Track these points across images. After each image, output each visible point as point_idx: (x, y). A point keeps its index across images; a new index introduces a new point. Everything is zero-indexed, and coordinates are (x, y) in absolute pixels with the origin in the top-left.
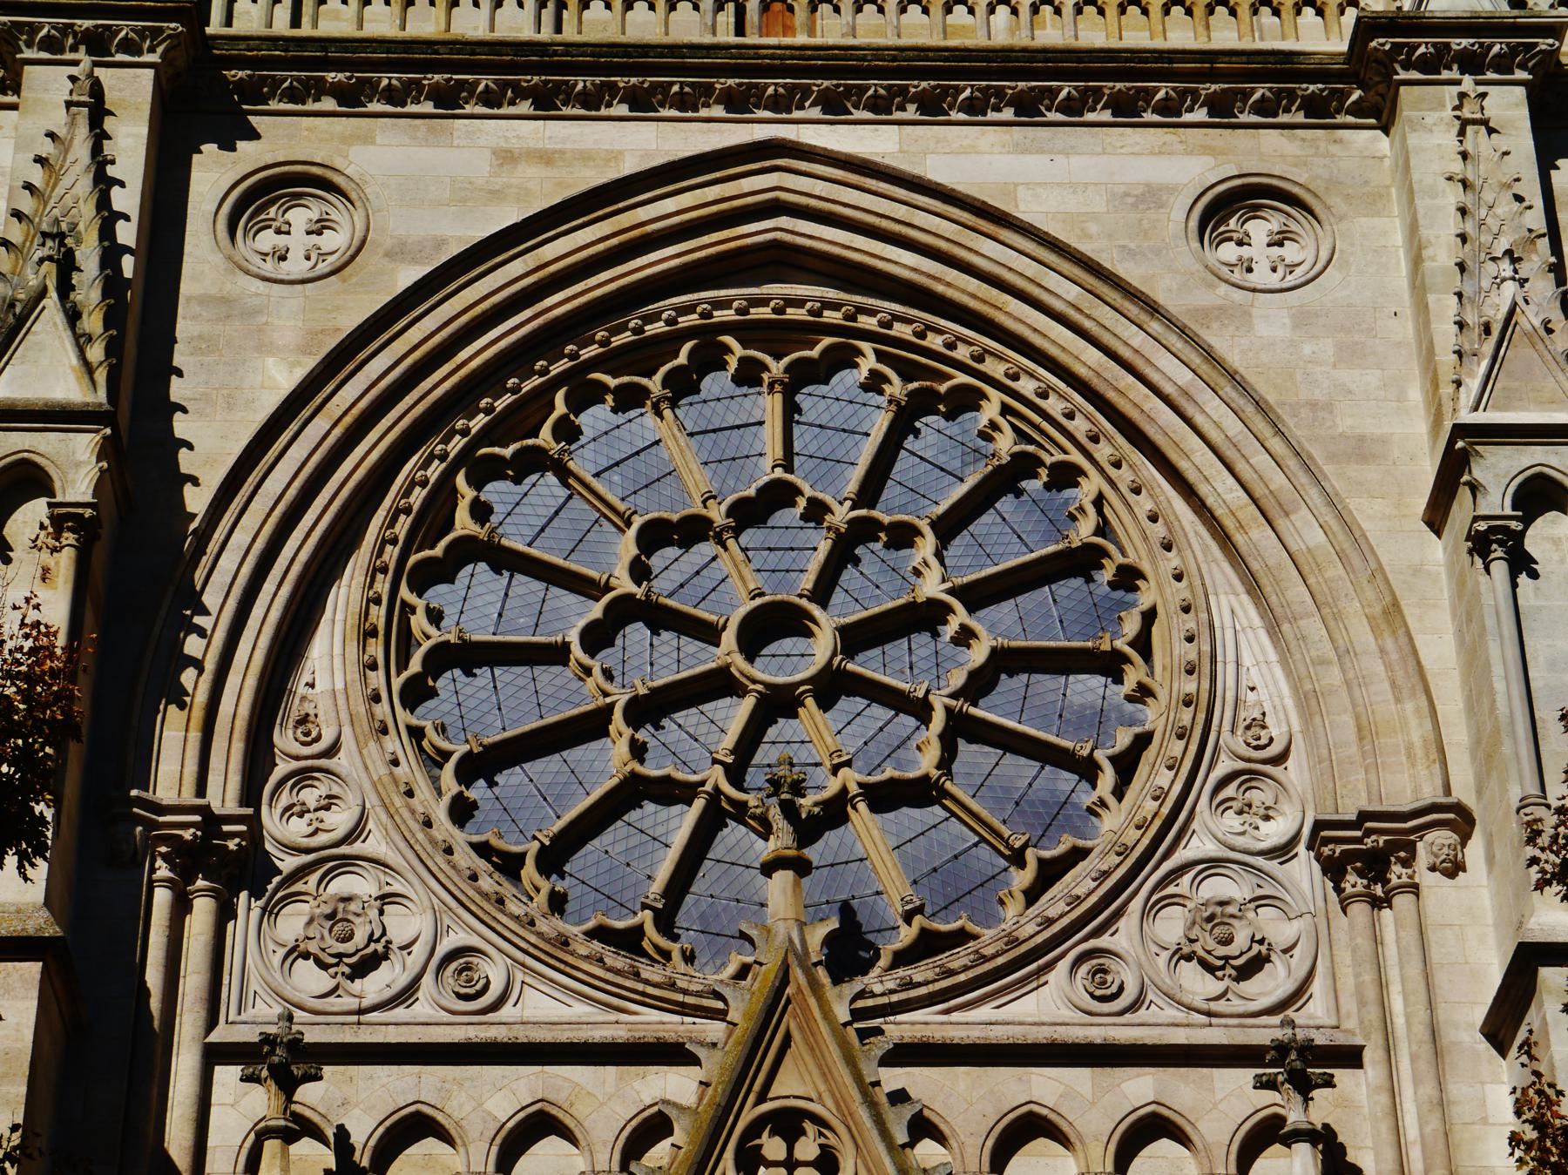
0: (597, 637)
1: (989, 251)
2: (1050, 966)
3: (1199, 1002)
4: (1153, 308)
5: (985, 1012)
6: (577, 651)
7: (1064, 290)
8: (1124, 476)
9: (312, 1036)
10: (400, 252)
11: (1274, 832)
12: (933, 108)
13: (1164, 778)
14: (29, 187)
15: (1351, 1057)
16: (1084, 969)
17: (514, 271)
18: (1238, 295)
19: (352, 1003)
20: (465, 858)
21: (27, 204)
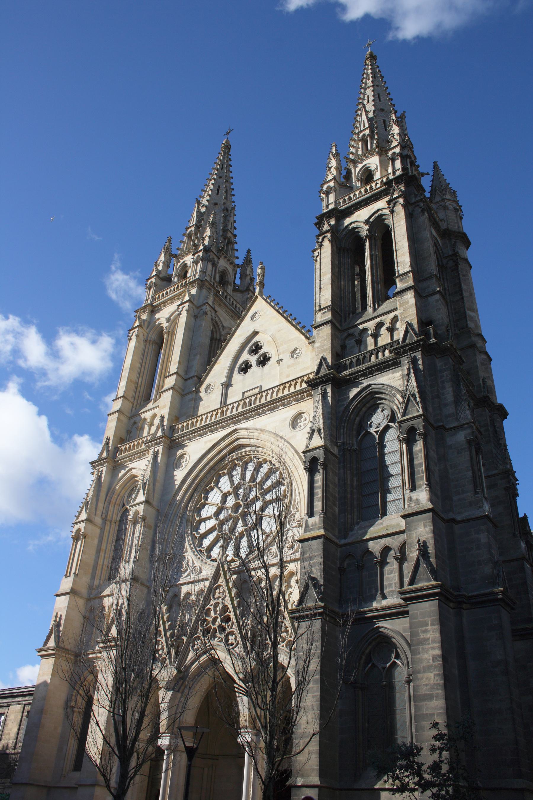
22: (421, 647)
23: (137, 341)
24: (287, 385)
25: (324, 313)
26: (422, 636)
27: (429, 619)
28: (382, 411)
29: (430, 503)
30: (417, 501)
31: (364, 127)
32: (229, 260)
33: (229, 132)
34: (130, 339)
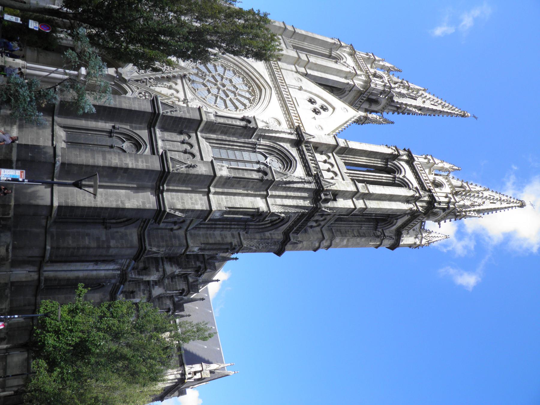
5: (188, 91)
22: (133, 158)
23: (331, 43)
24: (298, 118)
25: (344, 143)
26: (140, 160)
27: (149, 165)
28: (280, 168)
29: (220, 175)
30: (220, 170)
32: (386, 106)
33: (475, 118)
34: (332, 39)
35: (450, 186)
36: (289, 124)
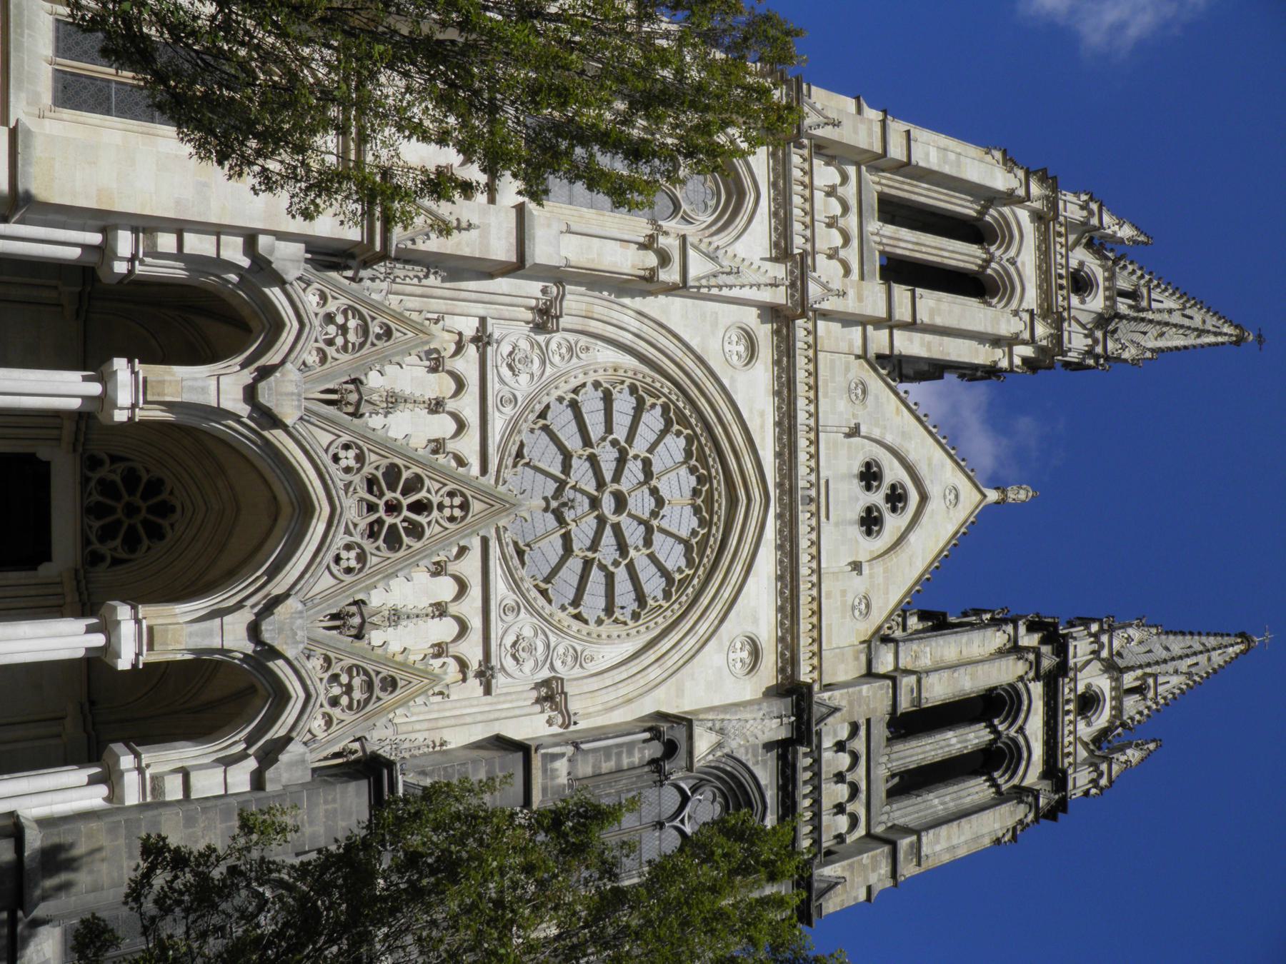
0: (615, 443)
1: (738, 568)
2: (514, 592)
3: (504, 642)
4: (722, 621)
5: (499, 571)
6: (611, 437)
7: (727, 593)
8: (669, 613)
9: (489, 349)
10: (733, 380)
11: (558, 664)
12: (779, 547)
13: (575, 628)
14: (752, 264)
15: (488, 691)
16: (514, 604)
17: (729, 416)
18: (726, 648)
19: (499, 364)
20: (545, 400)
21: (747, 263)
31: (1155, 300)
35: (1107, 293)
36: (783, 655)
